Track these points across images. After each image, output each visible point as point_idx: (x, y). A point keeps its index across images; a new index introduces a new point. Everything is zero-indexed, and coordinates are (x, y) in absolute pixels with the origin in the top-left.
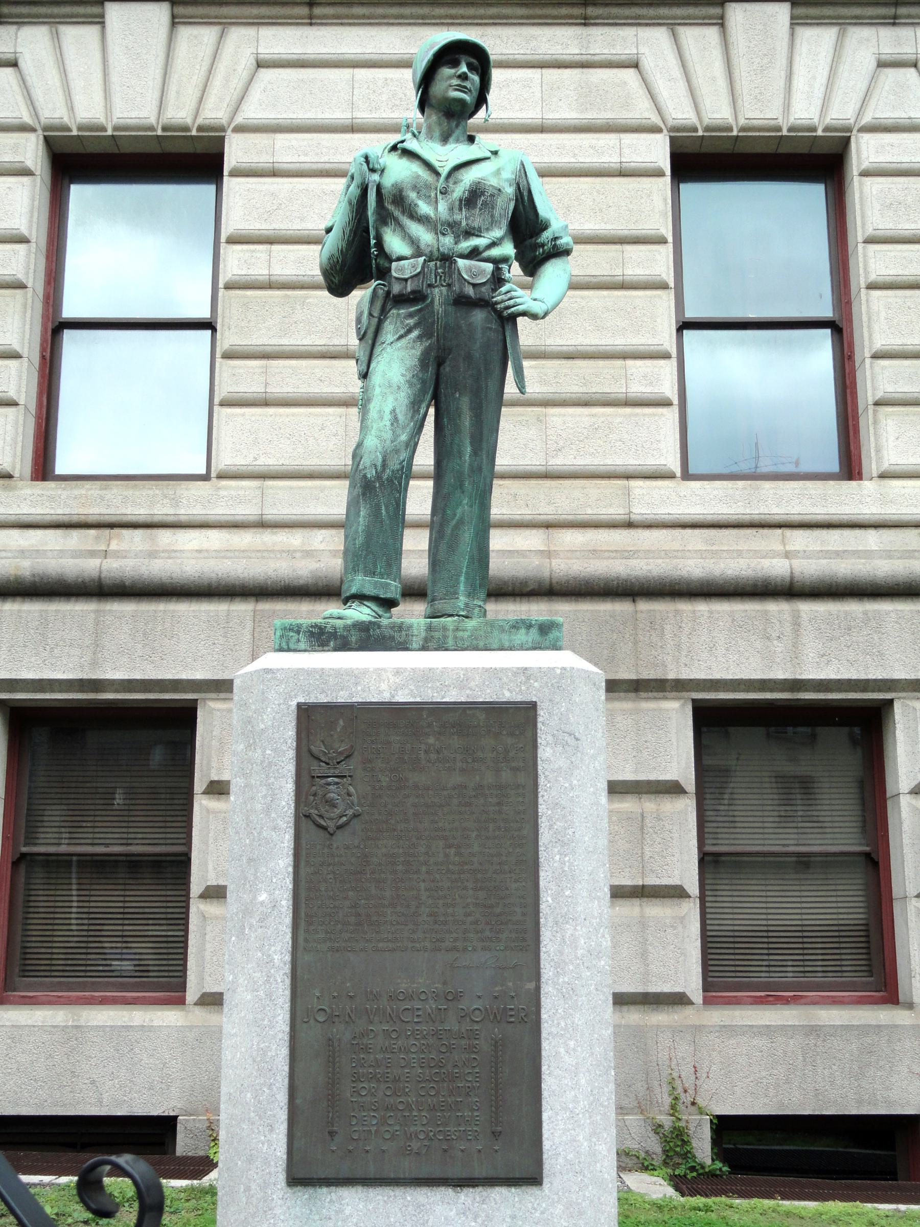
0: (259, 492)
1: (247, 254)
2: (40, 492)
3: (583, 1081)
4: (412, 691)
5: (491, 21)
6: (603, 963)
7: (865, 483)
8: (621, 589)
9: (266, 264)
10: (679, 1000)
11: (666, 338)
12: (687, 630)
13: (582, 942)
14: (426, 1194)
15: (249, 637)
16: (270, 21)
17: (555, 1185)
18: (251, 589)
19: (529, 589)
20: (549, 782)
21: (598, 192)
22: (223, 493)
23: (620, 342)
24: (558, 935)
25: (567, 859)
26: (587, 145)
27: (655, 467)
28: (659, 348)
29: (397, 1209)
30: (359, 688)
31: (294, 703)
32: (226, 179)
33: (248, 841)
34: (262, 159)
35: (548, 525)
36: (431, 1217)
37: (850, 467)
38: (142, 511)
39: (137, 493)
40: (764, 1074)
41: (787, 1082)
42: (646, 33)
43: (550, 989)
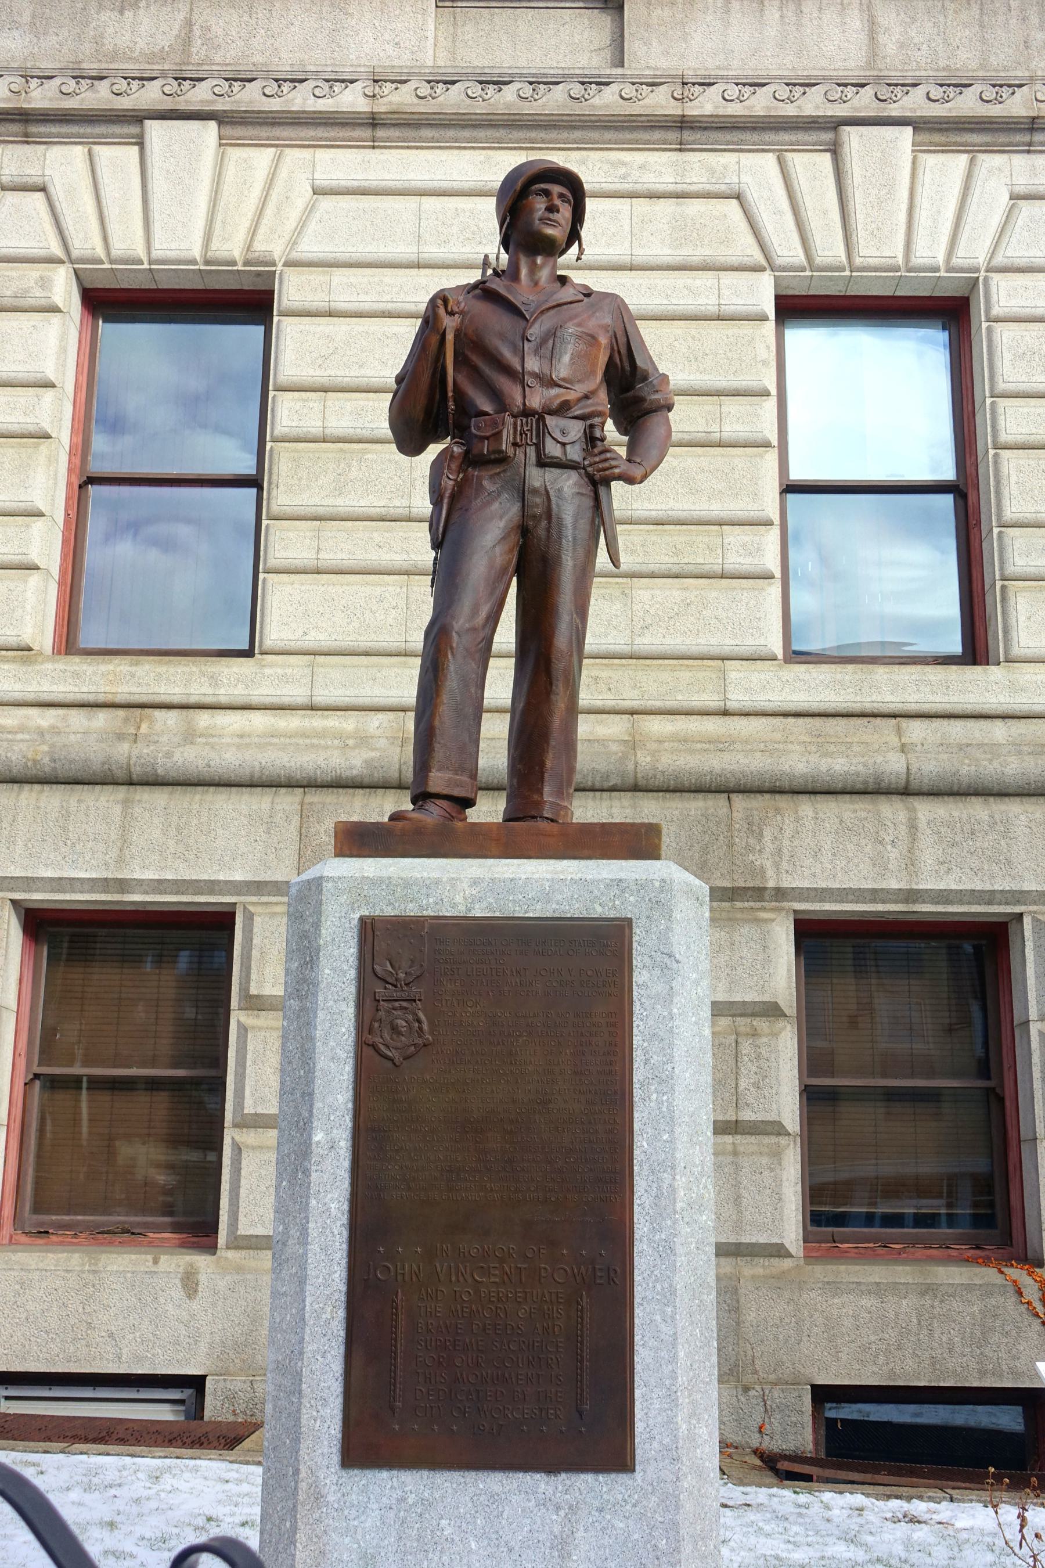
1: (300, 403)
2: (62, 667)
3: (682, 1354)
4: (490, 904)
5: (575, 146)
6: (705, 1218)
7: (992, 668)
9: (320, 416)
10: (779, 1251)
12: (788, 832)
13: (682, 1193)
14: (501, 1481)
17: (648, 1471)
18: (297, 781)
19: (611, 784)
20: (645, 1010)
21: (693, 338)
22: (268, 671)
23: (716, 508)
24: (655, 1185)
25: (665, 1098)
26: (681, 286)
27: (754, 648)
29: (467, 1498)
30: (431, 900)
31: (357, 916)
32: (275, 319)
33: (302, 1072)
35: (632, 713)
36: (506, 1508)
37: (977, 647)
38: (177, 690)
39: (172, 670)
40: (873, 1338)
41: (899, 1348)
43: (645, 1247)
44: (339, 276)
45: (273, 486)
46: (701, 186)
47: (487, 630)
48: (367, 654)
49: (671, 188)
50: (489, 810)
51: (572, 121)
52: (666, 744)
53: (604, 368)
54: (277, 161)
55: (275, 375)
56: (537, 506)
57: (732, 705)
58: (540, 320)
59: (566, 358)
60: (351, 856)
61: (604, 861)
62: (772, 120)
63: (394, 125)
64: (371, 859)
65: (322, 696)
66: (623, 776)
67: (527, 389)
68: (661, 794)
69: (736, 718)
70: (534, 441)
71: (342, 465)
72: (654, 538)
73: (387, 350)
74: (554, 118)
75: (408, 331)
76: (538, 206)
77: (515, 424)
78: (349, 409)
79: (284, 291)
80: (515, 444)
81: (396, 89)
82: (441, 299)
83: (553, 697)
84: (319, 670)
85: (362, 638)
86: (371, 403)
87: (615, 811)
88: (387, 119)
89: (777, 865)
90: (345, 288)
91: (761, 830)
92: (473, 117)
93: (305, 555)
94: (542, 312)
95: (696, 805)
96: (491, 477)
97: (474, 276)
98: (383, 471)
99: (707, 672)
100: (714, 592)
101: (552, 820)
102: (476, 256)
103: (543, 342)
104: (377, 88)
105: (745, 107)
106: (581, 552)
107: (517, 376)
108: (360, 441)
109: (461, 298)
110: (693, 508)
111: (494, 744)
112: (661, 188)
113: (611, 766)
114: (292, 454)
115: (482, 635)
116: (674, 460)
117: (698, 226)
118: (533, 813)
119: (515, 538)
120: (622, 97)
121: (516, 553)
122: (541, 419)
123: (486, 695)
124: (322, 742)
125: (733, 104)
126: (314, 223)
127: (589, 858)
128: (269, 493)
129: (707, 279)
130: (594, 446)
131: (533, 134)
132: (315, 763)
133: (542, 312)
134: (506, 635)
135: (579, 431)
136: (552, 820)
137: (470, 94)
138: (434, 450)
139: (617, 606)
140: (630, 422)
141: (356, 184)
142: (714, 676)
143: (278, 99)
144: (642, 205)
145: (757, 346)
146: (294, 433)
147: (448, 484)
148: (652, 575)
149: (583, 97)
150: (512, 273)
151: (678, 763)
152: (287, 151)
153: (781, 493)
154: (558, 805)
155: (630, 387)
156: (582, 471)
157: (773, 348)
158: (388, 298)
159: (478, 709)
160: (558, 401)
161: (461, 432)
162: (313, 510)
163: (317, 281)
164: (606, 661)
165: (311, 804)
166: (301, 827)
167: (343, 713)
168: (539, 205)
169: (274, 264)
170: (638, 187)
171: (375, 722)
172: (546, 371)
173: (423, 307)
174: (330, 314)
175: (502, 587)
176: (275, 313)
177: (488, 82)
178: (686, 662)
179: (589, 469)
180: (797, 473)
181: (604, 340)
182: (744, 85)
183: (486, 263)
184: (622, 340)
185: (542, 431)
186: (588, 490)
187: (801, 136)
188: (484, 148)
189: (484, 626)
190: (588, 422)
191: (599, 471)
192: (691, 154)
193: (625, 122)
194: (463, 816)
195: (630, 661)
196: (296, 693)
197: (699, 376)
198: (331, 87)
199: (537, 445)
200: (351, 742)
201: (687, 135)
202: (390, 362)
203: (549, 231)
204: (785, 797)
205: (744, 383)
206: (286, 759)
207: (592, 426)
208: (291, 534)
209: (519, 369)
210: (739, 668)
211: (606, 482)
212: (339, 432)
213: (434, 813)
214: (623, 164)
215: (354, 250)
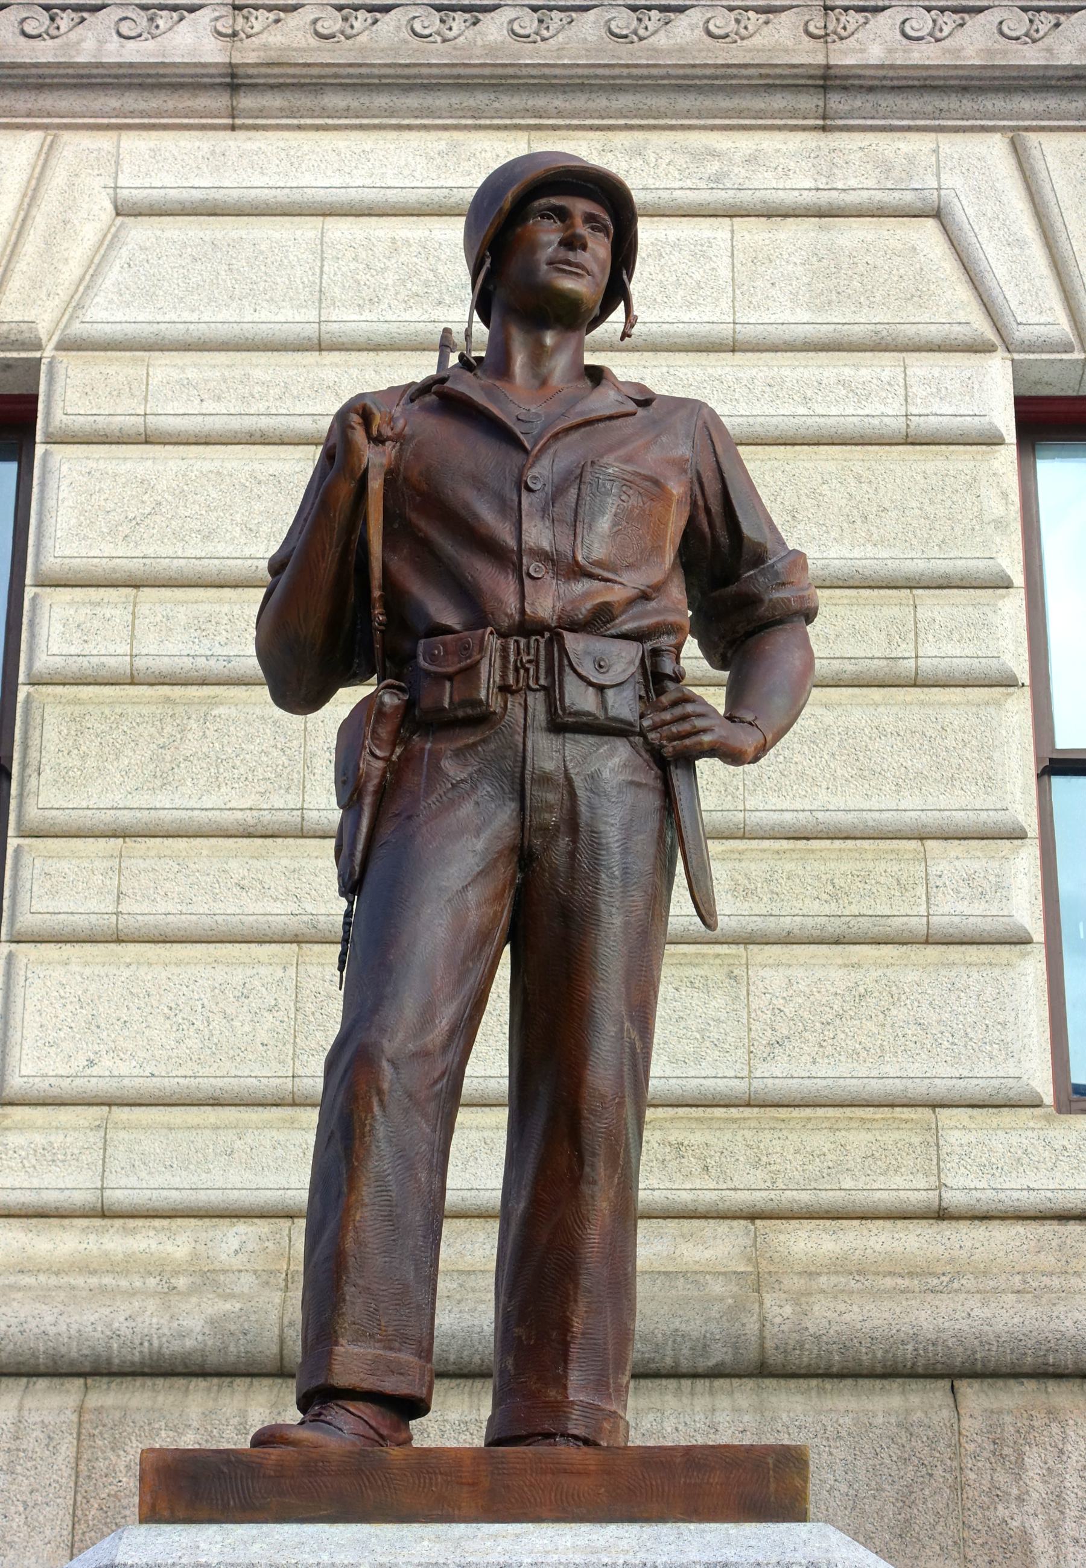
0: (95, 1138)
1: (86, 610)
5: (622, 122)
8: (921, 1362)
9: (126, 633)
11: (1018, 800)
15: (67, 1472)
16: (146, 121)
18: (72, 1363)
19: (711, 1362)
21: (859, 479)
23: (913, 806)
26: (832, 380)
27: (995, 1083)
28: (999, 816)
32: (39, 450)
34: (124, 413)
35: (753, 1216)
42: (952, 146)
44: (165, 368)
45: (29, 771)
46: (865, 194)
47: (451, 1057)
48: (216, 1102)
49: (808, 198)
50: (458, 1421)
51: (614, 77)
52: (823, 1279)
53: (678, 540)
54: (46, 157)
55: (37, 555)
56: (550, 808)
57: (954, 1198)
58: (551, 451)
59: (604, 524)
60: (173, 1520)
61: (692, 1526)
62: (997, 73)
63: (272, 87)
64: (214, 1527)
65: (123, 1190)
66: (735, 1347)
67: (527, 581)
68: (814, 1382)
69: (963, 1225)
70: (542, 682)
71: (168, 729)
72: (789, 866)
73: (258, 506)
74: (580, 71)
75: (299, 467)
76: (545, 238)
77: (505, 650)
78: (182, 619)
79: (57, 397)
80: (505, 689)
81: (277, 21)
82: (359, 413)
83: (585, 1189)
84: (119, 1136)
85: (206, 1071)
86: (226, 609)
87: (722, 1418)
88: (258, 76)
89: (1054, 1527)
90: (177, 392)
91: (1021, 1455)
92: (425, 71)
93: (93, 905)
94: (556, 437)
95: (885, 1404)
96: (459, 753)
97: (421, 368)
98: (250, 739)
99: (898, 1134)
100: (913, 969)
101: (586, 1442)
102: (431, 326)
103: (558, 492)
104: (240, 20)
105: (945, 51)
106: (638, 898)
107: (508, 559)
108: (203, 683)
109: (397, 411)
110: (866, 805)
111: (468, 1285)
112: (789, 198)
113: (712, 1326)
114: (69, 709)
115: (440, 1066)
116: (820, 711)
117: (861, 268)
118: (548, 1427)
119: (504, 872)
120: (709, 34)
121: (508, 901)
122: (556, 638)
123: (449, 1183)
124: (124, 1283)
125: (922, 46)
126: (116, 268)
127: (661, 1518)
128: (22, 785)
129: (882, 368)
130: (660, 691)
131: (540, 101)
132: (109, 1325)
133: (556, 437)
134: (490, 1062)
135: (632, 662)
136: (586, 1442)
137: (418, 27)
138: (346, 700)
139: (719, 1001)
140: (732, 643)
141: (197, 195)
142: (916, 1140)
143: (50, 42)
144: (753, 233)
145: (983, 492)
146: (74, 666)
147: (373, 767)
148: (788, 940)
149: (635, 32)
150: (498, 364)
151: (847, 1317)
152: (66, 136)
153: (1039, 776)
154: (599, 1409)
155: (730, 576)
156: (638, 740)
157: (1015, 497)
158: (262, 408)
159: (435, 1212)
160: (589, 605)
161: (395, 665)
162: (108, 816)
163: (121, 378)
164: (698, 1112)
165: (99, 1410)
166: (78, 1459)
167: (165, 1222)
168: (548, 236)
169: (39, 347)
170: (745, 197)
171: (231, 1241)
172: (565, 546)
173: (326, 423)
174: (147, 439)
175: (481, 967)
176: (39, 437)
177: (453, 8)
178: (859, 1112)
179: (652, 736)
180: (1069, 738)
181: (677, 488)
182: (942, 10)
183: (445, 344)
184: (712, 488)
185: (558, 662)
186: (649, 777)
187: (1053, 102)
188: (445, 128)
189: (445, 1048)
190: (649, 645)
191: (672, 738)
192: (845, 135)
193: (716, 78)
194: (403, 1436)
195: (747, 1112)
196: (70, 1183)
197: (870, 551)
198: (151, 19)
199: (548, 690)
200: (182, 1282)
201: (837, 102)
202: (265, 529)
203: (568, 284)
204: (1066, 1385)
205: (959, 563)
206: (49, 1319)
207: (656, 653)
208: (64, 865)
209: (512, 543)
210: (966, 1122)
211: (687, 760)
212: (164, 665)
213: (344, 1430)
214: (714, 154)
215: (194, 317)
